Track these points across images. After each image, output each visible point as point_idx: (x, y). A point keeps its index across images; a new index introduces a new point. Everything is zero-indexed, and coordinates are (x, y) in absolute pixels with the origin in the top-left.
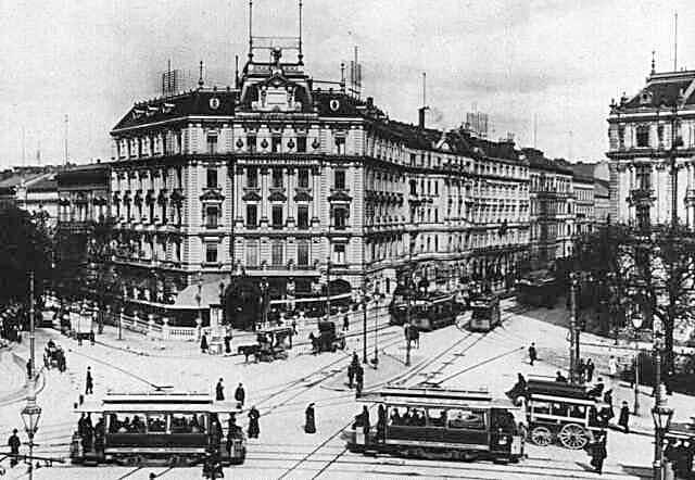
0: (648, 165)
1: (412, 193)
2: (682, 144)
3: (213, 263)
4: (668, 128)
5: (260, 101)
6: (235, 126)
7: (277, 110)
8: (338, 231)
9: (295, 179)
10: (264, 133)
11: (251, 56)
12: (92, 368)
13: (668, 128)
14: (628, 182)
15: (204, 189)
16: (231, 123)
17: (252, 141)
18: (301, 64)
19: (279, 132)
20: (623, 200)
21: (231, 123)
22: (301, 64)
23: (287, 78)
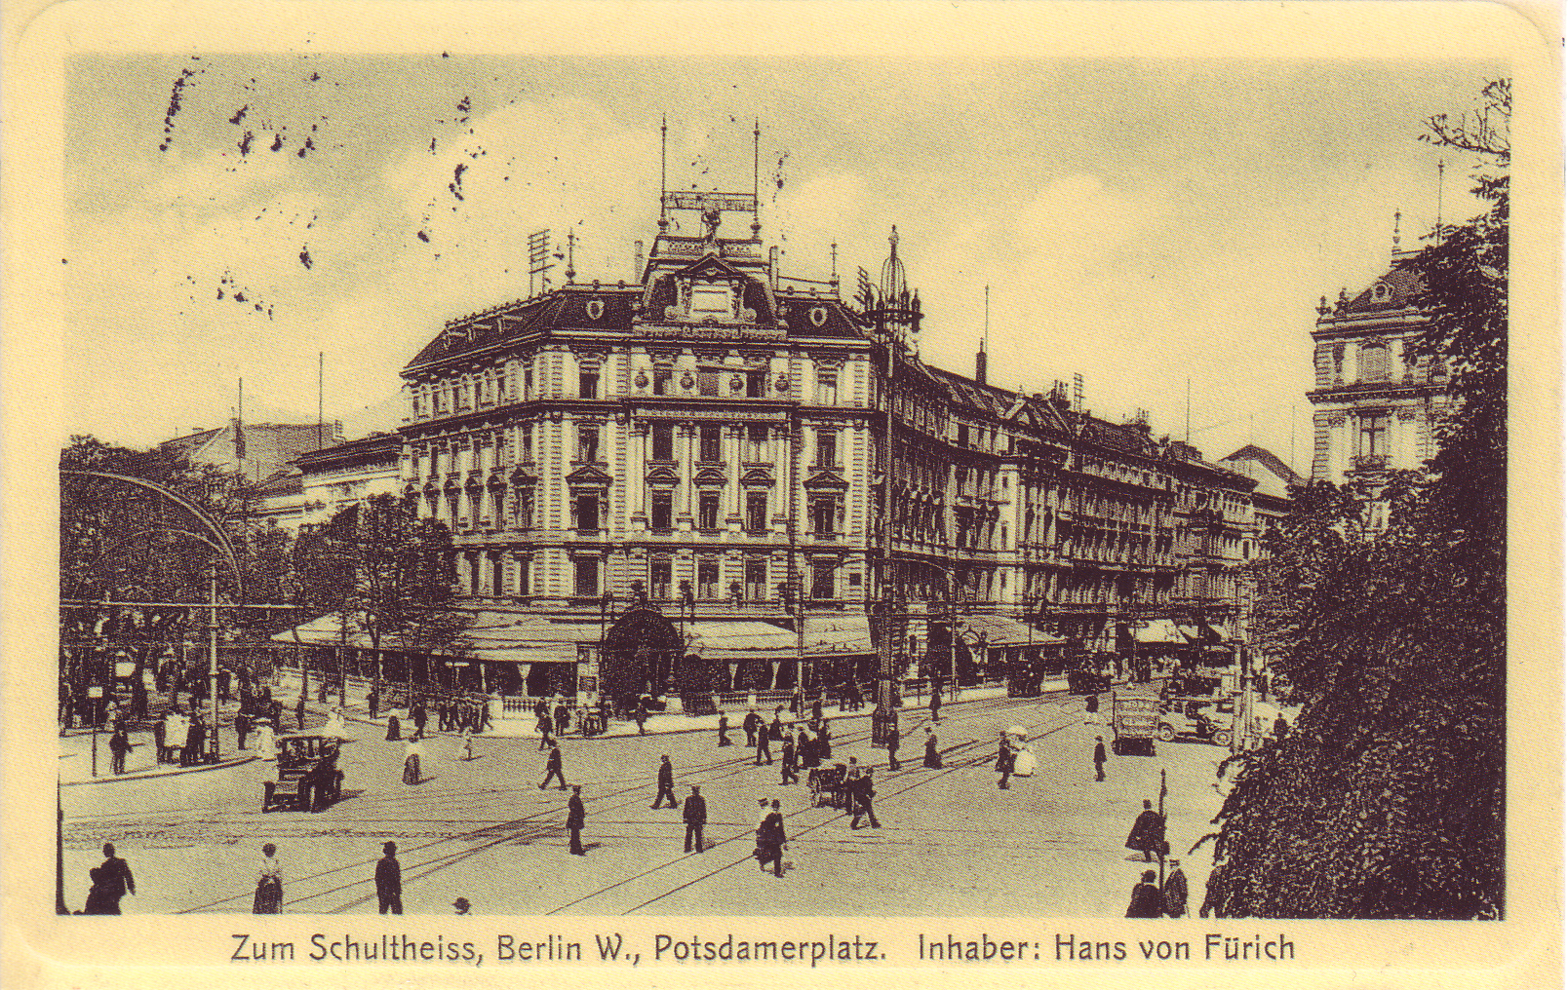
6: (633, 349)
11: (1396, 240)
18: (756, 240)
22: (756, 240)
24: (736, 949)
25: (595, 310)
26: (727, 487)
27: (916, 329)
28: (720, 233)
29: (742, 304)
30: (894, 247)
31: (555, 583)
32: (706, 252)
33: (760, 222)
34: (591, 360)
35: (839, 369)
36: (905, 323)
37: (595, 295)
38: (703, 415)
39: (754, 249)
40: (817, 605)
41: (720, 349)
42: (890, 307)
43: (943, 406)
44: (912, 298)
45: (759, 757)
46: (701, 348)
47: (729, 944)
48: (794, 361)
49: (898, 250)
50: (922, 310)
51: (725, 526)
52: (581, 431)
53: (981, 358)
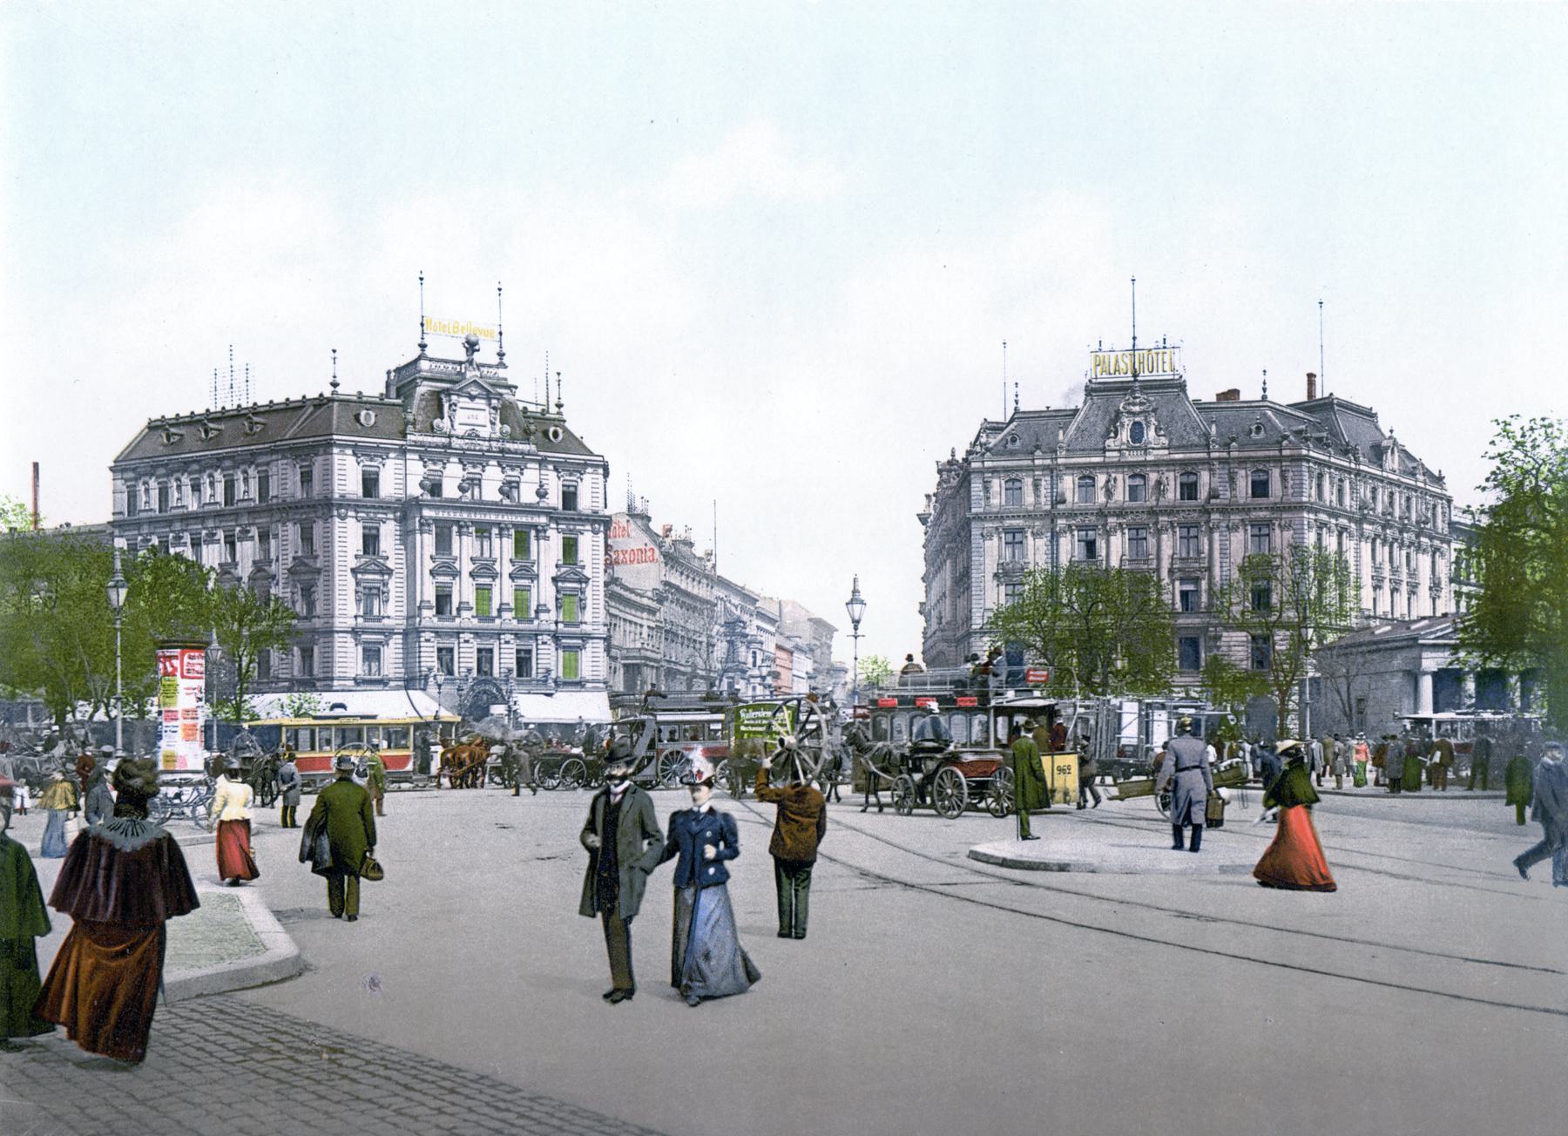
0: (1021, 530)
2: (1064, 502)
4: (1045, 483)
5: (446, 419)
6: (408, 456)
7: (473, 436)
8: (368, 624)
9: (509, 544)
13: (1045, 483)
14: (996, 553)
15: (356, 557)
16: (403, 452)
18: (502, 365)
19: (438, 467)
20: (989, 577)
21: (403, 452)
22: (502, 365)
23: (495, 393)
26: (498, 580)
29: (498, 422)
31: (595, 659)
33: (504, 350)
34: (372, 463)
35: (381, 466)
38: (479, 517)
40: (565, 684)
41: (481, 459)
46: (464, 458)
48: (543, 472)
52: (364, 528)
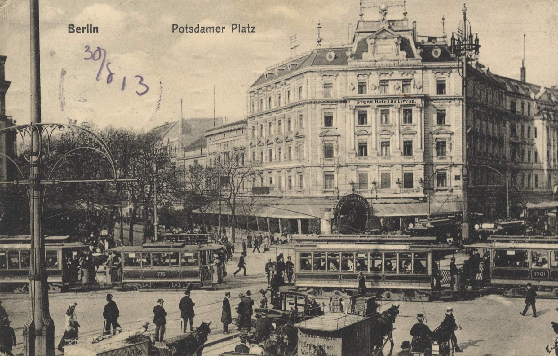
1: (511, 136)
3: (384, 108)
10: (374, 79)
12: (281, 94)
17: (362, 87)
18: (406, 19)
22: (406, 19)
24: (200, 29)
25: (330, 57)
27: (477, 52)
28: (388, 17)
30: (465, 14)
32: (381, 26)
36: (471, 50)
37: (330, 50)
39: (405, 23)
42: (464, 43)
43: (502, 93)
44: (474, 39)
45: (346, 182)
47: (198, 27)
49: (467, 15)
50: (480, 44)
51: (393, 154)
53: (523, 69)
